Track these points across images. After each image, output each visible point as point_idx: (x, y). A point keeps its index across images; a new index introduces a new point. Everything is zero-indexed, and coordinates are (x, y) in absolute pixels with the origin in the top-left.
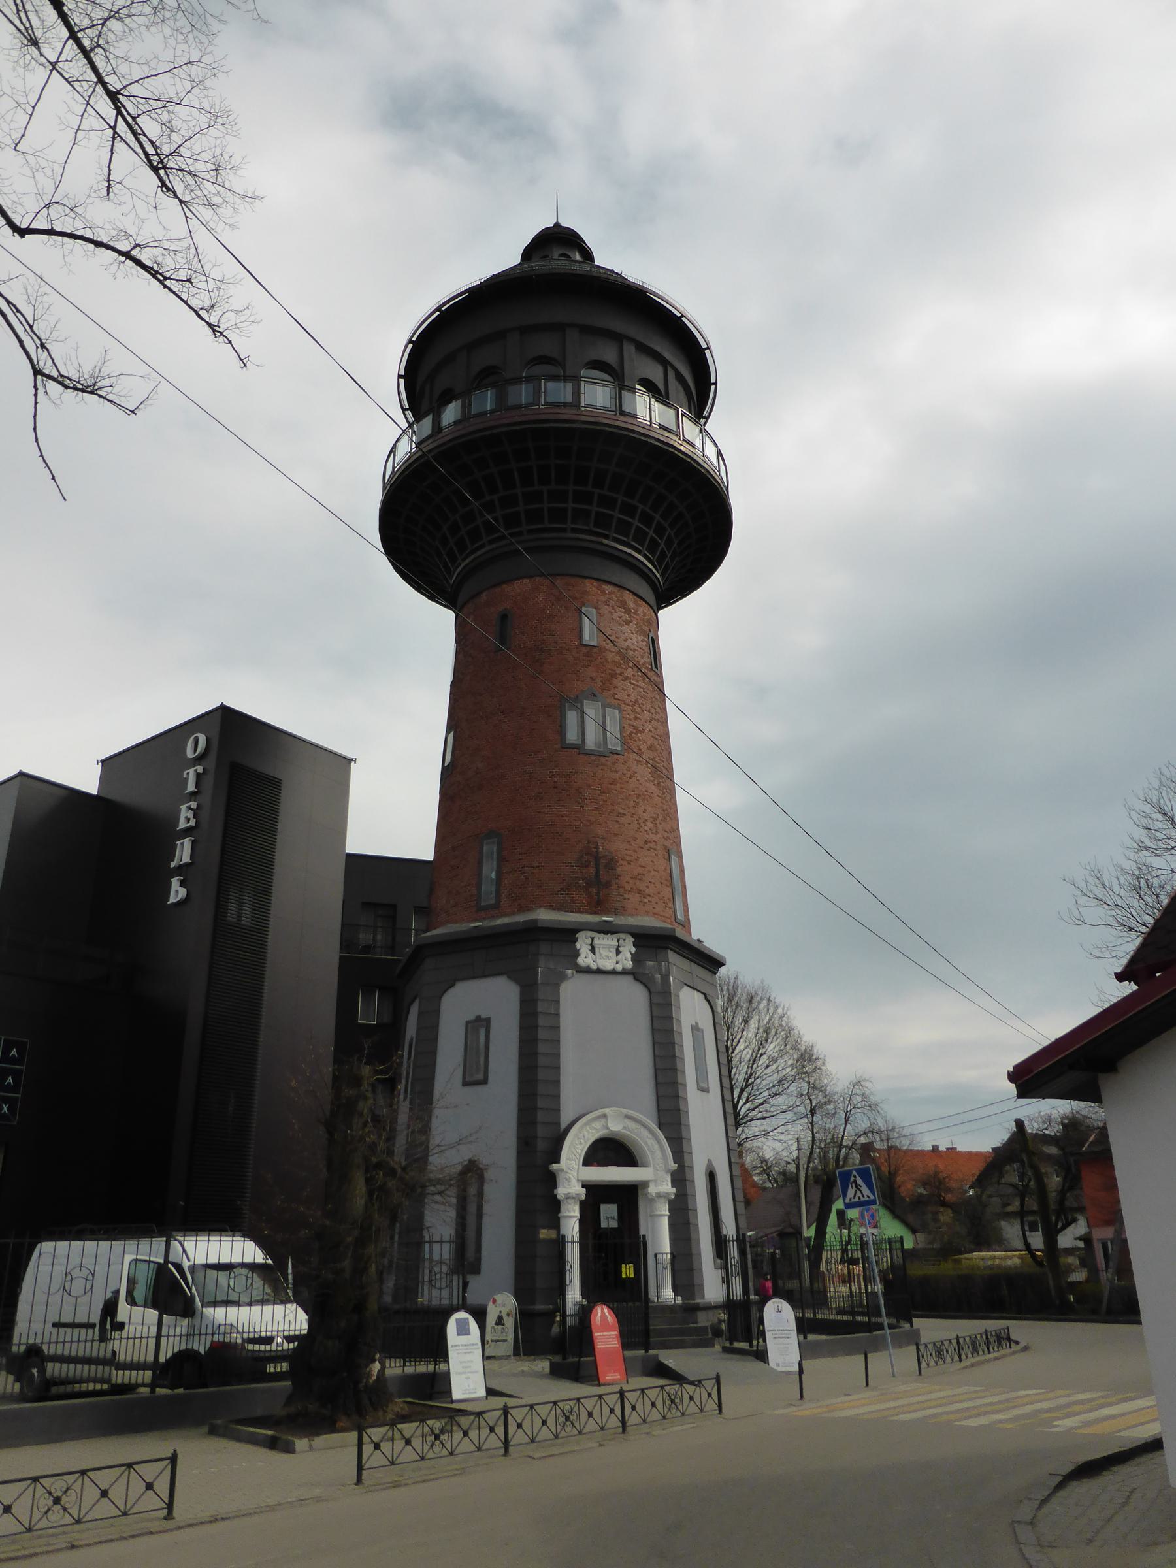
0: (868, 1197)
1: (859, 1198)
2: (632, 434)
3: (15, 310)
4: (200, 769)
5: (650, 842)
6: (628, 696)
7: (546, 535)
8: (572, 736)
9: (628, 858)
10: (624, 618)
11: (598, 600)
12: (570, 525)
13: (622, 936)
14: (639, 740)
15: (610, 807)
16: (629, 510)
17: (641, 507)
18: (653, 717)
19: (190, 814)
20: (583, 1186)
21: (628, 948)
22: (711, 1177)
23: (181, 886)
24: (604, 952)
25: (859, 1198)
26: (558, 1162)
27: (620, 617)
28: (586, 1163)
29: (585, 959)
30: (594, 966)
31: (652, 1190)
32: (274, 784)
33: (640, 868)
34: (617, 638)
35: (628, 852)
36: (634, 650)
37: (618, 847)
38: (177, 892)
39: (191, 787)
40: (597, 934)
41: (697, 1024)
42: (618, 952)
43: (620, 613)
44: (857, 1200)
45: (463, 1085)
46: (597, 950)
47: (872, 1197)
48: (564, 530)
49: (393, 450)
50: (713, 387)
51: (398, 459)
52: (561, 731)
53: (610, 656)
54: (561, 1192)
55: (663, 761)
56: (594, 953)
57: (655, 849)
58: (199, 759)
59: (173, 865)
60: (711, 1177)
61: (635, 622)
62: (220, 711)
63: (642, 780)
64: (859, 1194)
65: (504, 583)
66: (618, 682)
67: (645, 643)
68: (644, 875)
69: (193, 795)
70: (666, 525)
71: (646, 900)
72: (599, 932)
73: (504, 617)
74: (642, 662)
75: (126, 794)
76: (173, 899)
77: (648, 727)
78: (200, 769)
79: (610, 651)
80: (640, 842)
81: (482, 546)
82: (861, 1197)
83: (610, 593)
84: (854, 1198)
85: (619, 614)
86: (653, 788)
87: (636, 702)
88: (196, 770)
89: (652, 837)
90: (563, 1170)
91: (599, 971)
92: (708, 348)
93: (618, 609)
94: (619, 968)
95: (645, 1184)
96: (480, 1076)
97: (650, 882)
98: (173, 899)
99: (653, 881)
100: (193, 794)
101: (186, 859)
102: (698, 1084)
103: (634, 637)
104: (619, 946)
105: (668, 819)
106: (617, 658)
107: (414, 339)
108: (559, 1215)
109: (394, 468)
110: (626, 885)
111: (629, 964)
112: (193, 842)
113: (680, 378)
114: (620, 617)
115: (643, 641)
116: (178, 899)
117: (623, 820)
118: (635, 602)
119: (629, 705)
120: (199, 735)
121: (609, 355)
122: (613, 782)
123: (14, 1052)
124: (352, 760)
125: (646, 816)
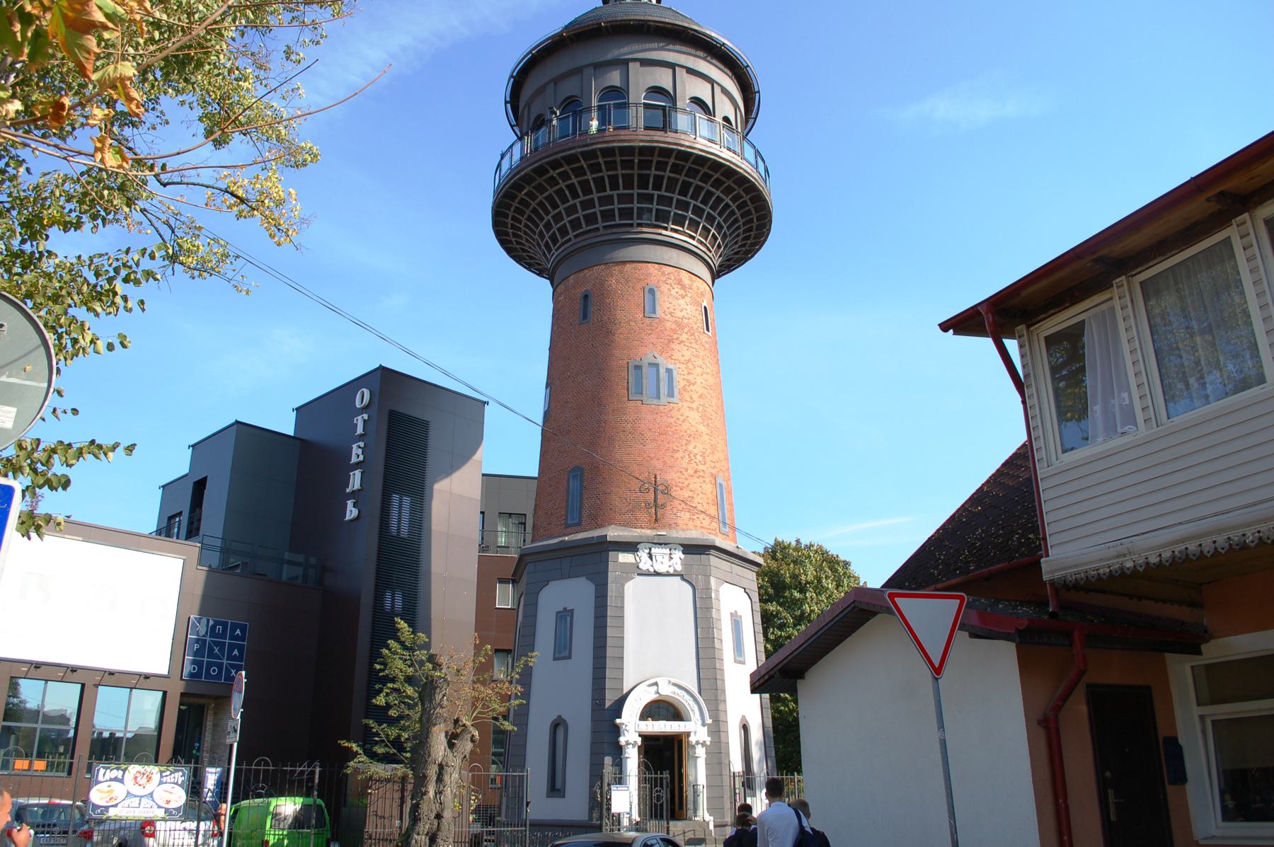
2: (680, 148)
4: (366, 416)
5: (699, 472)
6: (683, 356)
7: (586, 236)
9: (680, 485)
10: (680, 293)
11: (659, 280)
12: (571, 235)
13: (674, 546)
14: (691, 391)
15: (667, 445)
17: (693, 202)
18: (704, 371)
19: (360, 451)
20: (640, 736)
22: (745, 728)
23: (354, 507)
26: (621, 718)
27: (677, 293)
31: (693, 739)
32: (423, 425)
33: (690, 492)
34: (675, 310)
35: (681, 480)
36: (689, 319)
37: (672, 477)
38: (351, 511)
39: (360, 430)
40: (653, 545)
41: (736, 612)
43: (677, 289)
45: (554, 660)
46: (654, 557)
48: (631, 225)
49: (499, 165)
50: (757, 95)
53: (668, 325)
54: (622, 740)
55: (712, 406)
56: (652, 560)
57: (703, 477)
59: (348, 491)
60: (745, 728)
61: (689, 295)
62: (379, 371)
63: (693, 423)
65: (587, 268)
66: (675, 346)
67: (698, 312)
68: (693, 497)
69: (361, 437)
71: (695, 517)
73: (586, 297)
74: (695, 327)
76: (348, 517)
77: (699, 380)
79: (668, 321)
83: (669, 274)
85: (676, 290)
86: (702, 428)
87: (689, 360)
88: (363, 417)
89: (701, 467)
90: (623, 724)
91: (657, 574)
93: (675, 286)
95: (688, 734)
96: (566, 653)
97: (699, 503)
98: (348, 517)
99: (701, 502)
100: (361, 435)
102: (735, 659)
103: (688, 307)
104: (671, 554)
105: (715, 451)
106: (674, 326)
107: (515, 74)
108: (622, 757)
109: (500, 180)
110: (678, 506)
112: (362, 473)
114: (677, 293)
115: (696, 310)
116: (352, 517)
117: (677, 455)
118: (691, 280)
119: (683, 363)
120: (364, 389)
122: (670, 425)
124: (485, 402)
125: (696, 451)
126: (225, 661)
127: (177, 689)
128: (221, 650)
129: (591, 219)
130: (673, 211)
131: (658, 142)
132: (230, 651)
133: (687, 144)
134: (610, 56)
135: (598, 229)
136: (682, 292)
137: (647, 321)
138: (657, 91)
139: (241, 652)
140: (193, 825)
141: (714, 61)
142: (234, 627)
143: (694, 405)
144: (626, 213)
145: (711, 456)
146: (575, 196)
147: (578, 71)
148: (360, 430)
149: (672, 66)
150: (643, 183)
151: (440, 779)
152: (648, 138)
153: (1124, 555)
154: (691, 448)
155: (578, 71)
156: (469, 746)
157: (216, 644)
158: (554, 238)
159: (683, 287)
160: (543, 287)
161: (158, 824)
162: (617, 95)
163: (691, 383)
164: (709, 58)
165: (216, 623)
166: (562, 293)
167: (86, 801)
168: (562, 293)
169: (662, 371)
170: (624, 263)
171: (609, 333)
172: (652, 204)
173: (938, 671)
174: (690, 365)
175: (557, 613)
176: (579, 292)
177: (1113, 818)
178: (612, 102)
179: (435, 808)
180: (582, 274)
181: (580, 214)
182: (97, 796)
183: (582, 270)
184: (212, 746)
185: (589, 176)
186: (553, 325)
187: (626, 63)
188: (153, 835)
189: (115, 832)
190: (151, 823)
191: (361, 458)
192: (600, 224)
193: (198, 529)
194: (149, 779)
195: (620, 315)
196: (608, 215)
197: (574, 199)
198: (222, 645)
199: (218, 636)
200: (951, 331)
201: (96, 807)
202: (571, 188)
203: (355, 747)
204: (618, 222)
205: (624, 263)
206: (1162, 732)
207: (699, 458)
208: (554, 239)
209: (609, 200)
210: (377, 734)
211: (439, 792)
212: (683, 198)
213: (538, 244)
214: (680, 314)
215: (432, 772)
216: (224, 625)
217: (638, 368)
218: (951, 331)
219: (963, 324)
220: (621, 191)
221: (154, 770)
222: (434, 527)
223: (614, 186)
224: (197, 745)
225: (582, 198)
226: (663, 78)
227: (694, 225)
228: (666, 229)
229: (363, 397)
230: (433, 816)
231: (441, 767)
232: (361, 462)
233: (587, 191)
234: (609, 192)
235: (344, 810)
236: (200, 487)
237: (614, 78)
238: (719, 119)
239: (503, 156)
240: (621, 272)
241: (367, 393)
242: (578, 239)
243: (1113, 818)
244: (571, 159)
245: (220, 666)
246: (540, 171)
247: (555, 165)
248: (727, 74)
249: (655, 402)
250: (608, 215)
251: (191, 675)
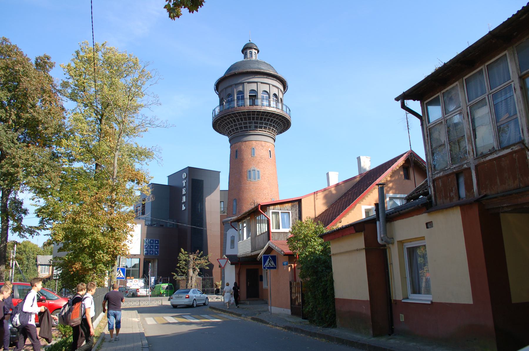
0: (274, 266)
1: (270, 266)
3: (401, 212)
12: (239, 131)
16: (274, 126)
19: (185, 191)
25: (270, 266)
39: (184, 185)
47: (275, 266)
48: (247, 130)
64: (119, 275)
73: (237, 151)
80: (264, 199)
81: (232, 134)
82: (271, 265)
87: (264, 167)
89: (267, 197)
106: (260, 158)
113: (281, 90)
123: (157, 247)
125: (266, 193)
126: (154, 250)
127: (142, 258)
128: (153, 247)
129: (237, 129)
130: (259, 125)
131: (251, 109)
132: (155, 247)
133: (259, 109)
134: (239, 82)
135: (239, 132)
136: (262, 148)
137: (252, 158)
138: (253, 91)
139: (158, 247)
140: (146, 290)
141: (270, 78)
142: (156, 241)
143: (265, 180)
144: (246, 127)
146: (232, 123)
147: (231, 86)
148: (184, 185)
149: (257, 82)
150: (249, 119)
151: (191, 279)
152: (248, 109)
154: (264, 192)
155: (231, 86)
156: (197, 273)
157: (151, 245)
159: (263, 146)
161: (139, 290)
162: (241, 93)
163: (264, 174)
164: (268, 77)
165: (151, 240)
167: (126, 286)
169: (256, 172)
170: (246, 141)
171: (242, 162)
174: (264, 169)
176: (235, 150)
177: (248, 285)
178: (240, 95)
179: (191, 285)
181: (238, 126)
182: (128, 285)
185: (235, 118)
187: (243, 83)
188: (139, 292)
189: (131, 292)
190: (138, 289)
191: (185, 193)
192: (239, 131)
194: (137, 281)
195: (245, 157)
196: (241, 128)
197: (241, 121)
198: (153, 246)
199: (151, 243)
201: (128, 287)
202: (231, 121)
203: (175, 274)
204: (244, 130)
205: (246, 141)
206: (260, 274)
207: (267, 194)
209: (241, 124)
210: (179, 271)
211: (191, 282)
214: (262, 155)
215: (190, 278)
216: (153, 240)
217: (250, 171)
220: (244, 121)
221: (138, 280)
222: (207, 210)
223: (242, 120)
225: (234, 124)
226: (254, 87)
227: (265, 128)
228: (257, 130)
229: (184, 175)
230: (190, 286)
231: (191, 277)
233: (235, 121)
234: (240, 122)
235: (176, 286)
237: (240, 88)
240: (245, 144)
242: (242, 133)
243: (248, 285)
244: (229, 115)
245: (153, 251)
246: (222, 118)
247: (225, 116)
248: (274, 80)
249: (254, 180)
250: (241, 128)
251: (146, 254)
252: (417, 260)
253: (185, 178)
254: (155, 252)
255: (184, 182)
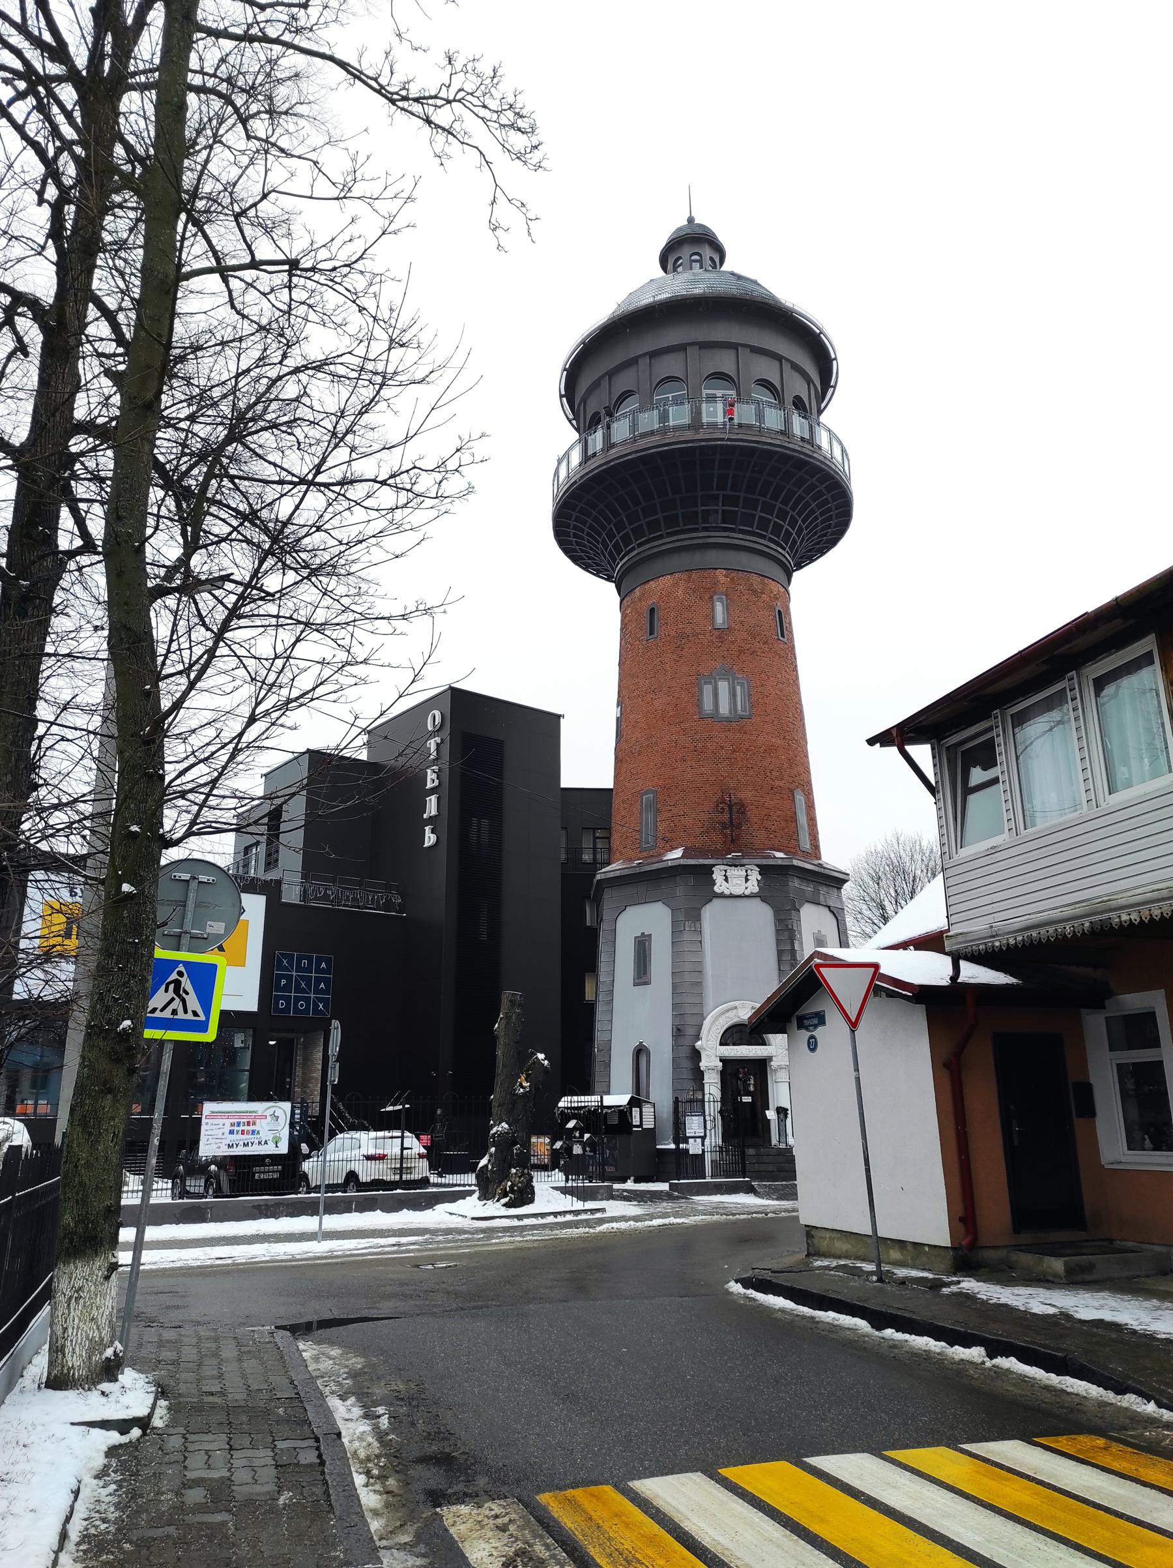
0: (195, 1014)
1: (174, 1012)
4: (438, 739)
8: (708, 705)
19: (434, 776)
20: (721, 1060)
21: (755, 876)
24: (735, 881)
25: (174, 1012)
28: (723, 1042)
29: (720, 886)
30: (727, 892)
31: (774, 1064)
42: (747, 880)
44: (167, 1014)
50: (835, 362)
51: (561, 480)
52: (699, 704)
54: (703, 1065)
58: (438, 731)
59: (425, 816)
64: (177, 1003)
65: (652, 580)
70: (788, 509)
72: (730, 866)
73: (652, 611)
75: (386, 757)
76: (426, 845)
78: (438, 739)
81: (633, 549)
84: (162, 1010)
89: (777, 783)
91: (732, 896)
92: (821, 333)
94: (747, 892)
95: (770, 1058)
98: (426, 845)
101: (434, 812)
111: (756, 889)
121: (727, 367)
145: (788, 770)
153: (993, 936)
158: (616, 546)
160: (604, 594)
166: (629, 606)
168: (629, 606)
172: (718, 505)
173: (854, 1025)
175: (636, 938)
176: (645, 606)
180: (647, 586)
183: (648, 581)
184: (304, 1080)
186: (621, 640)
193: (277, 860)
200: (878, 745)
208: (617, 547)
212: (750, 496)
213: (602, 552)
218: (878, 745)
219: (883, 739)
224: (288, 1080)
232: (436, 787)
236: (275, 816)
238: (789, 399)
239: (560, 462)
241: (437, 713)
245: (307, 1000)
252: (677, 428)
253: (436, 759)
254: (316, 1006)
255: (432, 744)
